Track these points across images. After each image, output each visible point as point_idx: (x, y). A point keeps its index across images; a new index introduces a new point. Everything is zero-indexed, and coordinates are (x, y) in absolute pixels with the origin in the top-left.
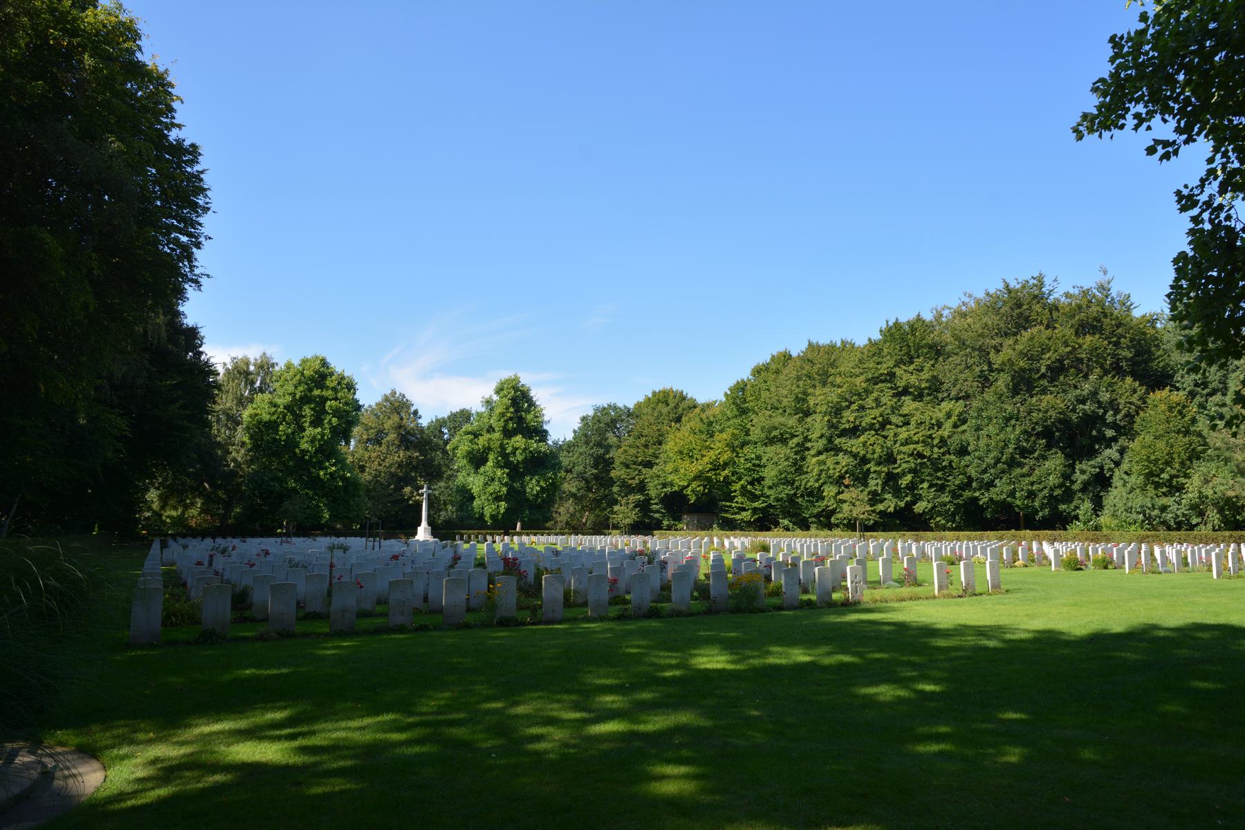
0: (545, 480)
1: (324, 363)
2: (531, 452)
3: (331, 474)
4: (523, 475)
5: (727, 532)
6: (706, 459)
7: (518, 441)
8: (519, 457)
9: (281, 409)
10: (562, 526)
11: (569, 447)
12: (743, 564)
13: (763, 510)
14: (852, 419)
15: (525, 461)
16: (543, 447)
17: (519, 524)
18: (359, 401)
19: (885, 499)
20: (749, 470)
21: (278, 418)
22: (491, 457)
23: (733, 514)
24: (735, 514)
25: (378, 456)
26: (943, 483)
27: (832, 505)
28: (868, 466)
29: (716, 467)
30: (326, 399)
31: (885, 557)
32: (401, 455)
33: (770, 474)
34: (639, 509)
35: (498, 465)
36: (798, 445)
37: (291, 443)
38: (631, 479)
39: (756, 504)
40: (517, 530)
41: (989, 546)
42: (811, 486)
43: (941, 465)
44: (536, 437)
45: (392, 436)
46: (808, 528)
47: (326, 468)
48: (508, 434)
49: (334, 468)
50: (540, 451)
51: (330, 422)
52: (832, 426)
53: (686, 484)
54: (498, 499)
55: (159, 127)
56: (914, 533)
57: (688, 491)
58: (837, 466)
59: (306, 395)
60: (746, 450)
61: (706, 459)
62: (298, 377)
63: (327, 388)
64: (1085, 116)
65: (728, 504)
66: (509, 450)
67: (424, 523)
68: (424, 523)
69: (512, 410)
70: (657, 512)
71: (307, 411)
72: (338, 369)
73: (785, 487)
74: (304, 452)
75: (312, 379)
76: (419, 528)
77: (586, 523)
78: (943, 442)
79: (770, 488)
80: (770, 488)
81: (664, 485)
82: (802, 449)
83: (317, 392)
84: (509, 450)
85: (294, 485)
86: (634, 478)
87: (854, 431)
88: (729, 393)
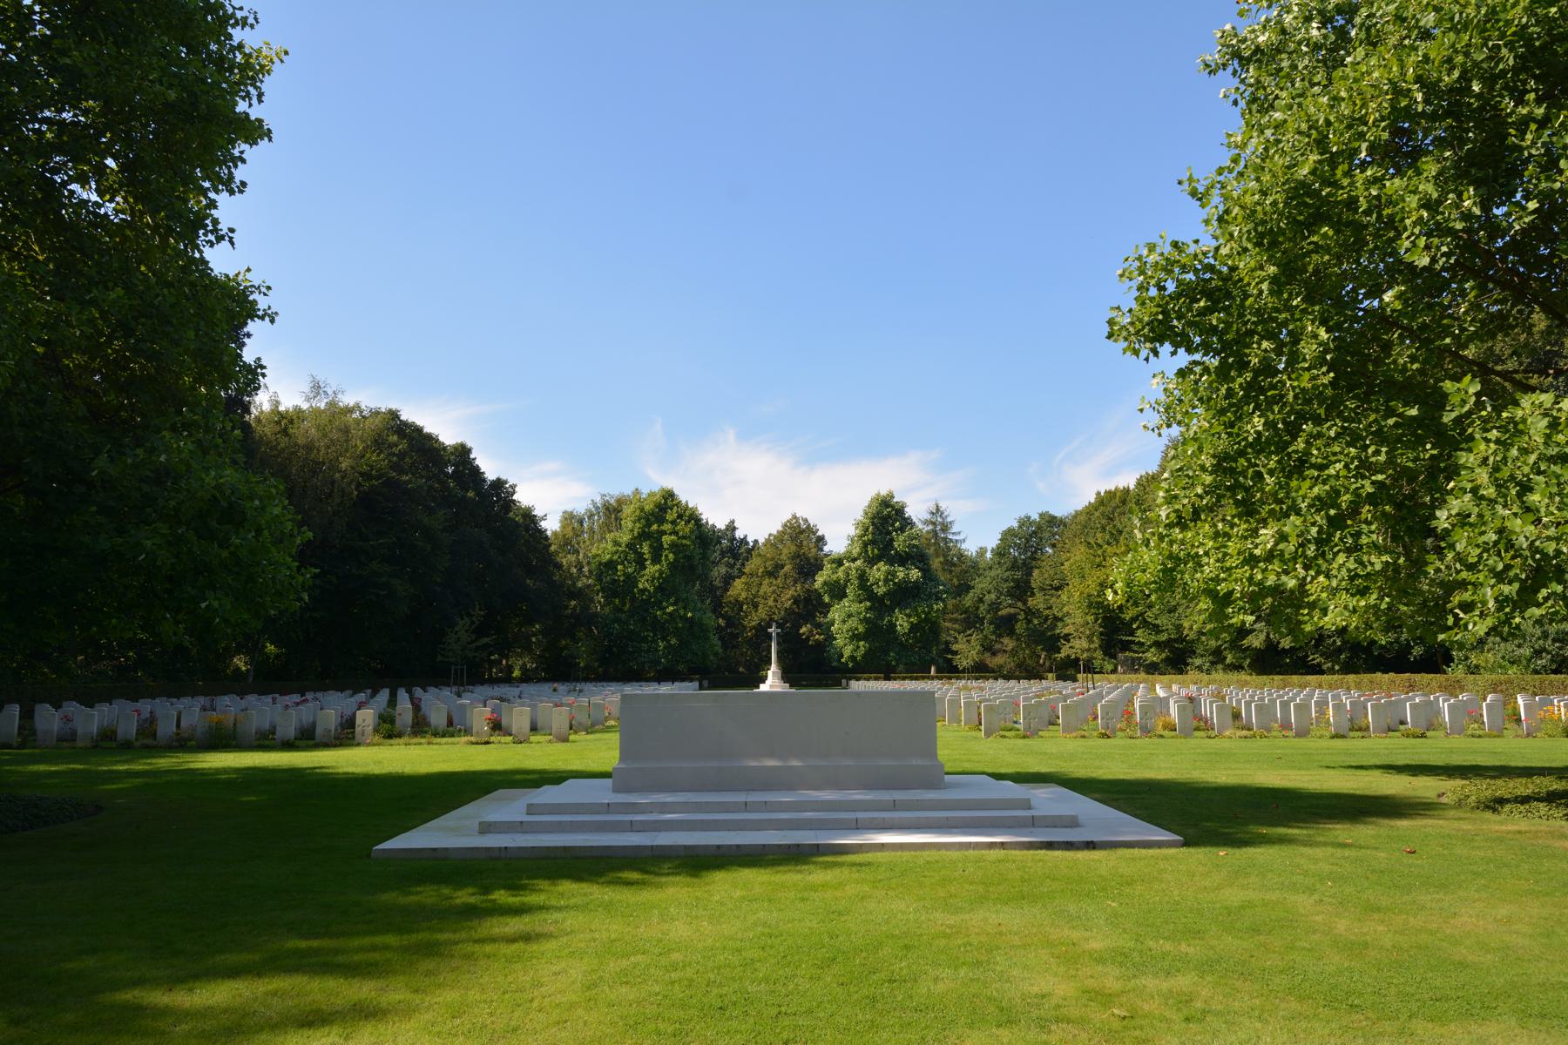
0: (918, 615)
3: (670, 614)
17: (933, 669)
18: (1029, 518)
25: (774, 592)
30: (664, 533)
37: (631, 581)
41: (1409, 699)
48: (872, 561)
55: (1406, 125)
59: (644, 532)
62: (638, 513)
64: (269, 72)
65: (1130, 638)
67: (774, 667)
68: (774, 667)
71: (646, 549)
77: (1044, 663)
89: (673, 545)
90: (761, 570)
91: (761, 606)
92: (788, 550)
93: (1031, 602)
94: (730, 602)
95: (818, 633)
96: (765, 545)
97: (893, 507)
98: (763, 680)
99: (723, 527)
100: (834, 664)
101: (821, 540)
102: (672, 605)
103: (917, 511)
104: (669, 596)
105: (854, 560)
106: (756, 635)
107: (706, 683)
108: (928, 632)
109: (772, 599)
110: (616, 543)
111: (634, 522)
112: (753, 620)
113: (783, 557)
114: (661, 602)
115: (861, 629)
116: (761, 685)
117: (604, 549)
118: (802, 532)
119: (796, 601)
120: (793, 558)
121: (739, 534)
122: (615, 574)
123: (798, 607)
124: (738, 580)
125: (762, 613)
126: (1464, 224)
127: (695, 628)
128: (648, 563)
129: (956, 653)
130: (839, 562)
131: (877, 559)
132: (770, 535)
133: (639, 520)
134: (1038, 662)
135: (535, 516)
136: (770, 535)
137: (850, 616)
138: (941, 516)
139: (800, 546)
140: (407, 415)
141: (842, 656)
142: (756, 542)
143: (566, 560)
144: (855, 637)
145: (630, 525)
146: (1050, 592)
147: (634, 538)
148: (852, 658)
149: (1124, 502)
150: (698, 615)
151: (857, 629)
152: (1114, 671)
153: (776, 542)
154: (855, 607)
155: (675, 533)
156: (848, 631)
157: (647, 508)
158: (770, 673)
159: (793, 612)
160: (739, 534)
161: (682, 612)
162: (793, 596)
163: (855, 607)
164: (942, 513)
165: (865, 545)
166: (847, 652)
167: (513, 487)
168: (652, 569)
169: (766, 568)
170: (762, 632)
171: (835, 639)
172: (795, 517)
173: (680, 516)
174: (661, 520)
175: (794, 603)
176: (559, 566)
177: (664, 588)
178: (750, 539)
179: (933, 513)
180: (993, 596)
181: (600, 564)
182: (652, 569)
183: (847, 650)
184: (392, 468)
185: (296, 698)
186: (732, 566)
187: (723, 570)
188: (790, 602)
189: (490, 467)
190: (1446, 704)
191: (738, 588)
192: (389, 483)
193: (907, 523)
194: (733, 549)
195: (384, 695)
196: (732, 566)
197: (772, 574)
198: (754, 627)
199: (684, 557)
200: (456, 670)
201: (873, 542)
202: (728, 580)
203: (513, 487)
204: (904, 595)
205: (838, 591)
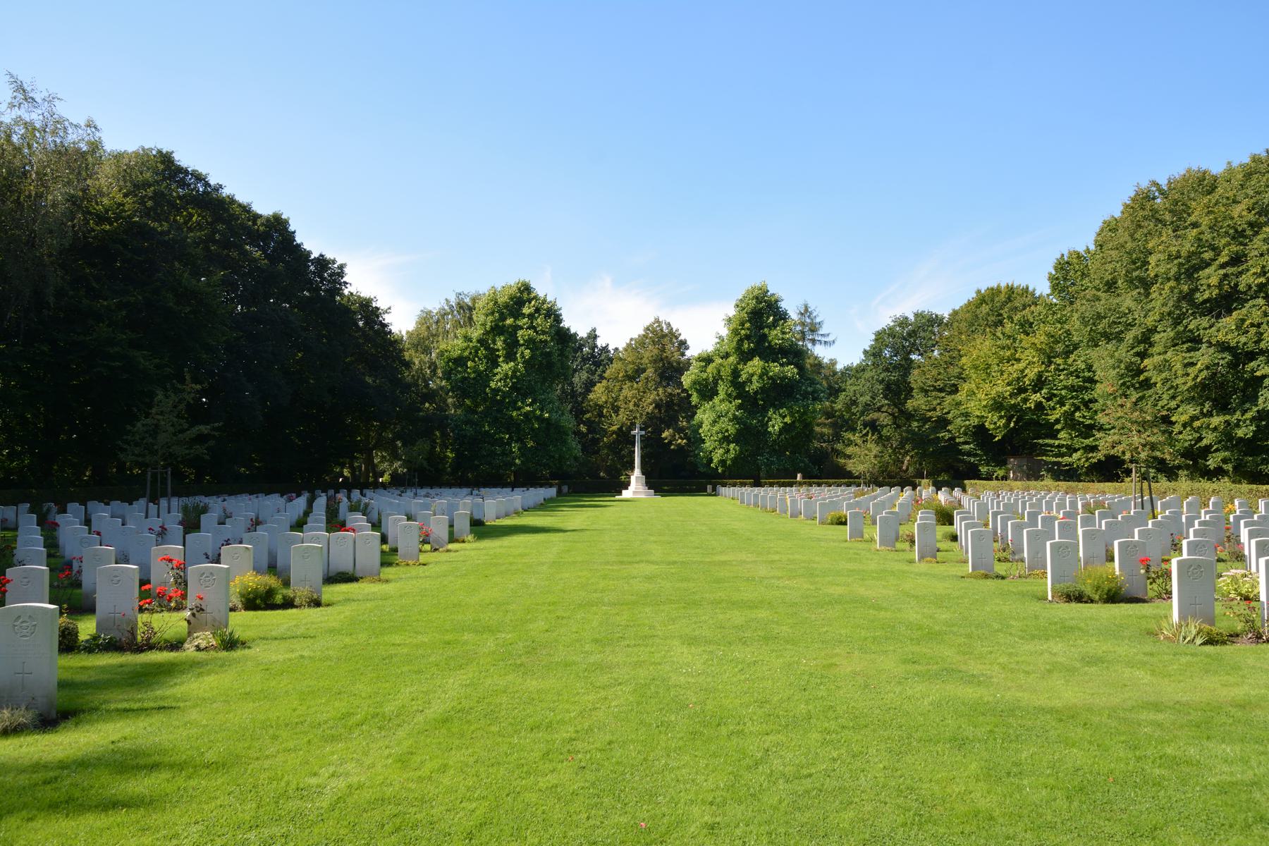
1: (526, 288)
3: (526, 415)
4: (764, 410)
7: (756, 364)
8: (755, 385)
9: (474, 344)
11: (853, 373)
12: (1025, 531)
14: (1214, 281)
15: (762, 390)
16: (683, 359)
17: (799, 475)
20: (1072, 388)
21: (471, 353)
23: (1056, 456)
24: (1062, 455)
28: (1253, 364)
31: (1057, 540)
32: (660, 392)
37: (483, 379)
38: (929, 411)
44: (782, 358)
45: (650, 372)
47: (519, 409)
48: (745, 357)
49: (528, 408)
50: (786, 377)
51: (523, 356)
58: (1190, 370)
59: (497, 325)
63: (523, 316)
66: (744, 377)
69: (747, 325)
70: (969, 454)
71: (499, 344)
72: (541, 294)
74: (496, 391)
75: (506, 306)
83: (509, 321)
84: (744, 377)
85: (487, 428)
86: (935, 409)
87: (1227, 301)
89: (530, 343)
90: (621, 375)
91: (622, 410)
92: (650, 353)
93: (910, 404)
95: (681, 438)
96: (626, 350)
98: (626, 485)
99: (585, 335)
101: (683, 345)
102: (530, 405)
103: (791, 307)
104: (525, 396)
105: (727, 356)
107: (565, 489)
108: (799, 433)
110: (467, 339)
111: (487, 315)
112: (617, 421)
113: (645, 361)
114: (515, 402)
116: (624, 492)
117: (454, 345)
118: (664, 336)
120: (655, 361)
121: (600, 343)
122: (465, 371)
124: (598, 385)
125: (622, 417)
126: (694, 423)
127: (552, 431)
128: (501, 359)
129: (849, 457)
130: (707, 360)
132: (631, 339)
133: (492, 313)
134: (901, 468)
135: (377, 309)
138: (809, 317)
139: (663, 350)
140: (185, 159)
141: (711, 460)
142: (616, 349)
143: (417, 359)
144: (726, 440)
145: (482, 318)
146: (934, 393)
147: (486, 333)
148: (723, 462)
149: (1009, 299)
150: (555, 416)
151: (727, 431)
152: (1005, 478)
153: (637, 346)
154: (724, 407)
155: (531, 327)
157: (501, 301)
158: (633, 479)
160: (600, 343)
161: (538, 412)
162: (654, 401)
163: (724, 407)
164: (811, 313)
165: (741, 341)
166: (717, 457)
167: (342, 267)
168: (505, 367)
169: (626, 371)
170: (625, 437)
172: (657, 321)
173: (537, 310)
174: (517, 314)
175: (655, 407)
176: (408, 365)
177: (520, 388)
178: (611, 348)
179: (802, 314)
180: (867, 398)
181: (450, 360)
182: (505, 367)
183: (717, 453)
184: (147, 213)
185: (525, 489)
186: (593, 373)
187: (584, 375)
188: (651, 407)
189: (312, 241)
191: (599, 394)
192: (142, 232)
193: (782, 316)
194: (599, 359)
195: (301, 502)
197: (632, 378)
198: (614, 432)
199: (542, 354)
200: (154, 476)
201: (748, 337)
202: (589, 386)
203: (342, 267)
204: (779, 392)
205: (707, 391)
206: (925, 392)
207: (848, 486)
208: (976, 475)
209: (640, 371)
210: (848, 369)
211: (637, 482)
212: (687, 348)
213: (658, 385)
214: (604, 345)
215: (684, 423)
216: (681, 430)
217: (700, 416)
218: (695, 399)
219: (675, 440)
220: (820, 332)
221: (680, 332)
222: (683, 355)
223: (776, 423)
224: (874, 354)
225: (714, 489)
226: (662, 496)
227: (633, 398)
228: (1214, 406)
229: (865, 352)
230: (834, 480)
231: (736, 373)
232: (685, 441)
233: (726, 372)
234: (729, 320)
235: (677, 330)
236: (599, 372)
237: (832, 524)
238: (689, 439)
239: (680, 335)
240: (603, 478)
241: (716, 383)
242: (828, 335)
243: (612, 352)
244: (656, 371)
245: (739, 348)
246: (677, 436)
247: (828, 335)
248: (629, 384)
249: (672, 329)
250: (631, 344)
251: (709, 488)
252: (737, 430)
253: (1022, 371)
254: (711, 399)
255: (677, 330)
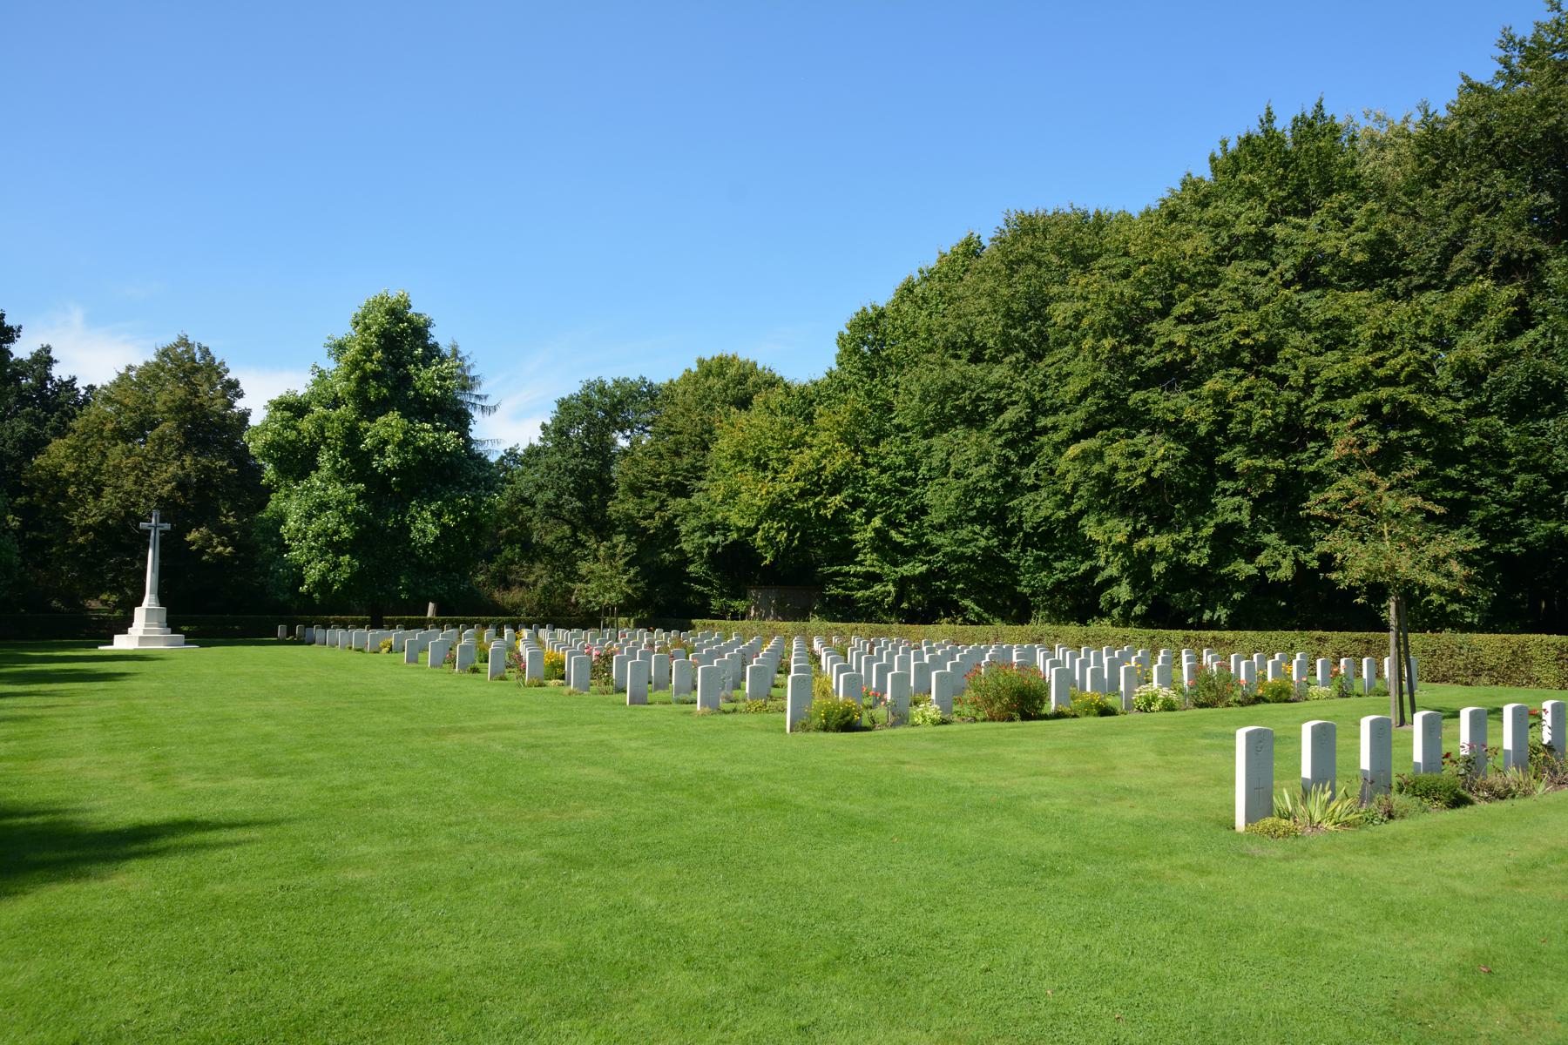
0: (455, 512)
2: (418, 450)
5: (840, 625)
6: (791, 471)
7: (391, 424)
10: (532, 609)
13: (923, 581)
15: (403, 470)
17: (431, 605)
19: (1266, 546)
22: (323, 458)
26: (1466, 498)
27: (1102, 563)
29: (816, 485)
32: (187, 463)
33: (940, 499)
34: (638, 568)
35: (340, 474)
36: (1015, 426)
38: (644, 518)
39: (906, 570)
40: (429, 615)
42: (1046, 519)
43: (1461, 445)
45: (167, 427)
46: (1023, 617)
48: (371, 409)
52: (1121, 361)
53: (753, 525)
54: (338, 548)
56: (1357, 635)
57: (758, 540)
60: (883, 447)
61: (791, 471)
67: (149, 600)
68: (149, 600)
69: (378, 354)
70: (698, 581)
73: (977, 528)
76: (137, 610)
78: (1471, 377)
79: (941, 528)
80: (941, 528)
81: (711, 529)
82: (1025, 436)
86: (651, 516)
87: (1175, 374)
88: (847, 332)
90: (110, 426)
91: (108, 490)
92: (169, 394)
94: (40, 480)
97: (410, 321)
98: (124, 625)
100: (283, 597)
105: (336, 403)
106: (93, 544)
109: (132, 478)
115: (346, 533)
116: (117, 637)
118: (197, 370)
119: (182, 485)
121: (59, 372)
123: (185, 495)
131: (381, 407)
132: (129, 368)
136: (129, 368)
137: (323, 506)
141: (302, 582)
148: (323, 584)
151: (336, 532)
156: (316, 537)
159: (175, 505)
160: (59, 372)
162: (175, 476)
163: (336, 491)
165: (363, 380)
166: (313, 573)
171: (287, 549)
186: (40, 423)
188: (168, 487)
190: (1053, 670)
196: (40, 423)
198: (89, 528)
206: (636, 490)
207: (407, 628)
208: (705, 613)
209: (144, 425)
210: (511, 454)
211: (148, 619)
212: (240, 395)
213: (183, 450)
214: (65, 379)
215: (231, 520)
216: (224, 530)
217: (275, 502)
218: (269, 472)
219: (211, 546)
220: (476, 392)
221: (227, 365)
222: (230, 405)
223: (425, 526)
224: (558, 431)
225: (291, 632)
226: (202, 646)
227: (133, 469)
228: (1150, 521)
229: (544, 427)
230: (488, 618)
231: (352, 436)
232: (229, 549)
233: (334, 432)
234: (341, 347)
235: (222, 364)
236: (53, 422)
237: (826, 729)
238: (237, 547)
239: (227, 371)
240: (57, 610)
241: (314, 450)
242: (486, 397)
243: (83, 392)
244: (180, 426)
245: (359, 395)
246: (215, 541)
247: (486, 397)
248: (121, 445)
249: (213, 359)
250: (129, 378)
251: (281, 630)
252: (356, 532)
253: (818, 462)
254: (304, 475)
255: (222, 364)
